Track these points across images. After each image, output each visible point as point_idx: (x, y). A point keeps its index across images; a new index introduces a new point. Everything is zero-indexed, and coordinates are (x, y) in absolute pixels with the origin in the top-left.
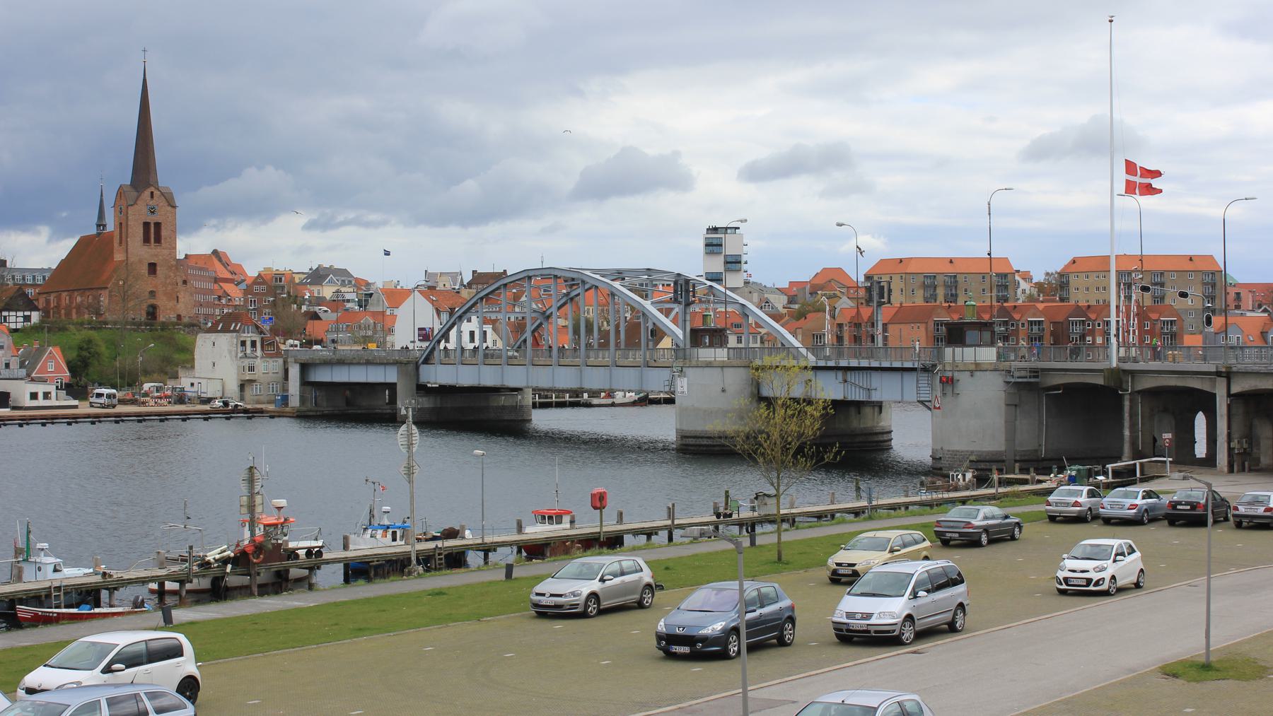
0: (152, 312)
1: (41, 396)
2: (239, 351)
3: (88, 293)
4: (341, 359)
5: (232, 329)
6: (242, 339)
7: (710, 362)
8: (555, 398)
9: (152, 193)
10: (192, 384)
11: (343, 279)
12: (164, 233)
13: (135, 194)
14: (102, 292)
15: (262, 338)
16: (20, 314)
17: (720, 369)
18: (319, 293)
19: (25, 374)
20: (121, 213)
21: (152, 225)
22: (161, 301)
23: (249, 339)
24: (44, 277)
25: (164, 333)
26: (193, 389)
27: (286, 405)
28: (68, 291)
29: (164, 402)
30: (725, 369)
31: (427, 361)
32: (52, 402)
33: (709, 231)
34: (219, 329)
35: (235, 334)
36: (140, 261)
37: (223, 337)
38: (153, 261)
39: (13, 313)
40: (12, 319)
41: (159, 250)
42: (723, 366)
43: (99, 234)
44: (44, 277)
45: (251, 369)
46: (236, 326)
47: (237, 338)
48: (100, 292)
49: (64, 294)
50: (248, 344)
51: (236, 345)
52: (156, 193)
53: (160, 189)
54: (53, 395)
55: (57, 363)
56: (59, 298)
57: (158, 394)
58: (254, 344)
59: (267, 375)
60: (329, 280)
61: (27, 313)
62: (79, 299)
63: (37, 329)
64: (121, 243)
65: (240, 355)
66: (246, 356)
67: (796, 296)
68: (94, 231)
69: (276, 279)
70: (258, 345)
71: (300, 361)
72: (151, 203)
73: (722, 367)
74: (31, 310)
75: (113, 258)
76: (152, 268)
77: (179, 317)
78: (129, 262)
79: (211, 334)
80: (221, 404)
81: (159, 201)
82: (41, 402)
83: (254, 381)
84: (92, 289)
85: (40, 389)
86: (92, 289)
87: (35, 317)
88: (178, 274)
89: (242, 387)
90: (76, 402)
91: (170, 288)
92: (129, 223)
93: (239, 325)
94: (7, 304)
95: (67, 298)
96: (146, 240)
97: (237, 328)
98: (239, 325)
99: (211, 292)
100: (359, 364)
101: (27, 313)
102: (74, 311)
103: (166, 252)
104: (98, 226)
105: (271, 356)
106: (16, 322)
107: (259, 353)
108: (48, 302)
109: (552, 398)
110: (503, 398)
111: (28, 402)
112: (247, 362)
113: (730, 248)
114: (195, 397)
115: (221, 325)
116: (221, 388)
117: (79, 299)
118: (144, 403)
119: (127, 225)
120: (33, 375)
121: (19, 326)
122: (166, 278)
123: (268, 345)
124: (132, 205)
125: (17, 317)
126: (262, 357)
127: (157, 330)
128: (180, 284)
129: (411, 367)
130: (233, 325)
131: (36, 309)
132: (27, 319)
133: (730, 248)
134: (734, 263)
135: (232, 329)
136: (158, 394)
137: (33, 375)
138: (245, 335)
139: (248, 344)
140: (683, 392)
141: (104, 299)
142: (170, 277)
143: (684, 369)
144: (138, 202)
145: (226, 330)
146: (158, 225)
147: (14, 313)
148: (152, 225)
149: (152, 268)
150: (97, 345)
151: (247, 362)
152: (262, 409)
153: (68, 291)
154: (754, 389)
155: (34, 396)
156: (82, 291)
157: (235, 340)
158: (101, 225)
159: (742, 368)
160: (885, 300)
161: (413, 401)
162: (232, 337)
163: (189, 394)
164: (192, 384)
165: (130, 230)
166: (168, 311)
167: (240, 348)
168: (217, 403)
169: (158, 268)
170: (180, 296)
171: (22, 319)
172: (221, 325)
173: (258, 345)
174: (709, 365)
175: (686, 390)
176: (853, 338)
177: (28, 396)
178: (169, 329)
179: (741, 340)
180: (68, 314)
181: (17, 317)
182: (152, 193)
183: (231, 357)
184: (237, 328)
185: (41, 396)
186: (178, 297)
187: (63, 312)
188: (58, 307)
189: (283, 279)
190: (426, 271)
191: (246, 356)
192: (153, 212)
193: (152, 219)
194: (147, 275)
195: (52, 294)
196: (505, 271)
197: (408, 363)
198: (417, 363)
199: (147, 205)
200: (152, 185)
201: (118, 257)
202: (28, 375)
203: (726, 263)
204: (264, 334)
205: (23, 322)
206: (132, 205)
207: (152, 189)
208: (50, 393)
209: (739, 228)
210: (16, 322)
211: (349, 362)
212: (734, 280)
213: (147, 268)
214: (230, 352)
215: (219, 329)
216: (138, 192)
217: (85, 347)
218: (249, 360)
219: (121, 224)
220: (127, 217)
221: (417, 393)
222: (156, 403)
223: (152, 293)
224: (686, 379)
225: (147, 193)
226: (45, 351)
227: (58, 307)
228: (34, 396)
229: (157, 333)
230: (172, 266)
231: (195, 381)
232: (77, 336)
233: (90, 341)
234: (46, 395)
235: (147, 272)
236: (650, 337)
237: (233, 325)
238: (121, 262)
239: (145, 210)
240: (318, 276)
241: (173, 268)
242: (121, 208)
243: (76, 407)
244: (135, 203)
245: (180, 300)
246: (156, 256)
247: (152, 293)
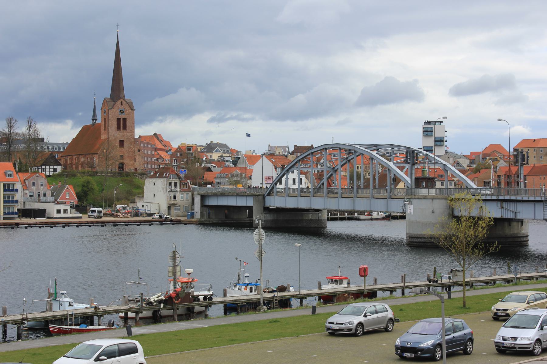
0: (122, 166)
1: (62, 211)
2: (168, 188)
3: (87, 156)
4: (223, 193)
5: (164, 176)
6: (170, 182)
7: (426, 196)
8: (340, 215)
9: (122, 102)
10: (143, 206)
11: (224, 149)
12: (128, 124)
13: (113, 103)
14: (95, 156)
15: (180, 181)
16: (51, 167)
17: (431, 200)
18: (211, 157)
19: (54, 199)
20: (105, 113)
21: (122, 120)
22: (126, 161)
23: (173, 182)
24: (64, 148)
25: (128, 178)
26: (143, 209)
27: (193, 217)
28: (77, 155)
29: (128, 215)
30: (434, 200)
31: (269, 195)
32: (69, 215)
33: (426, 124)
34: (157, 176)
35: (166, 179)
36: (115, 139)
37: (159, 180)
38: (122, 139)
39: (47, 167)
40: (47, 170)
41: (125, 133)
42: (433, 199)
43: (93, 125)
44: (64, 148)
45: (174, 198)
46: (166, 175)
47: (167, 181)
48: (94, 156)
49: (75, 157)
50: (173, 184)
51: (166, 185)
52: (124, 102)
53: (126, 100)
54: (69, 211)
55: (71, 194)
56: (72, 159)
57: (125, 211)
58: (176, 184)
59: (182, 201)
60: (216, 150)
61: (55, 167)
62: (83, 159)
63: (60, 175)
64: (105, 129)
65: (168, 190)
66: (171, 191)
67: (474, 160)
68: (90, 123)
69: (188, 149)
70: (178, 185)
71: (201, 194)
72: (121, 108)
73: (433, 199)
74: (57, 165)
75: (101, 137)
76: (122, 143)
77: (136, 169)
78: (109, 140)
79: (153, 179)
80: (158, 217)
81: (125, 107)
82: (62, 215)
83: (176, 204)
84: (90, 154)
85: (62, 207)
86: (90, 154)
87: (59, 169)
88: (135, 146)
89: (169, 207)
90: (81, 215)
91: (131, 154)
92: (109, 119)
93: (168, 174)
94: (45, 162)
95: (77, 159)
96: (118, 128)
97: (167, 176)
98: (168, 174)
99: (153, 156)
100: (232, 195)
101: (55, 167)
102: (80, 166)
103: (129, 134)
104: (93, 120)
105: (185, 191)
106: (49, 172)
107: (178, 189)
108: (66, 161)
109: (338, 215)
110: (311, 215)
111: (56, 215)
112: (172, 194)
113: (438, 133)
114: (144, 213)
115: (158, 174)
116: (158, 208)
117: (83, 159)
118: (117, 216)
119: (108, 120)
120: (58, 200)
121: (51, 174)
122: (129, 148)
123: (183, 185)
124: (111, 109)
125: (50, 169)
126: (180, 191)
127: (124, 176)
128: (136, 151)
129: (261, 198)
130: (165, 174)
131: (60, 165)
132: (55, 170)
133: (438, 133)
134: (439, 141)
135: (164, 176)
136: (125, 211)
137: (58, 200)
138: (171, 179)
139: (173, 184)
140: (410, 213)
141: (96, 160)
142: (131, 147)
143: (411, 200)
144: (114, 107)
145: (161, 177)
146: (125, 120)
147: (48, 167)
148: (122, 120)
149: (122, 143)
150: (92, 184)
151: (172, 194)
152: (180, 219)
153: (77, 155)
154: (450, 212)
155: (59, 211)
156: (84, 155)
157: (166, 182)
158: (94, 119)
159: (443, 200)
160: (525, 162)
161: (262, 216)
162: (164, 181)
163: (141, 211)
164: (143, 206)
165: (110, 123)
166: (130, 166)
167: (168, 187)
168: (156, 216)
169: (125, 143)
170: (136, 158)
171: (52, 170)
172: (158, 174)
173: (178, 185)
174: (425, 198)
175: (412, 211)
176: (506, 183)
177: (56, 211)
178: (131, 176)
179: (443, 184)
180: (77, 168)
181: (50, 169)
182: (122, 102)
183: (164, 191)
184: (167, 176)
185: (62, 211)
186: (135, 158)
187: (74, 166)
188: (71, 164)
189: (192, 149)
190: (269, 145)
191: (172, 191)
192: (122, 113)
193: (122, 116)
194: (119, 147)
195: (68, 157)
196: (312, 145)
197: (259, 195)
198: (264, 195)
199: (119, 109)
200: (122, 98)
201: (104, 137)
202: (56, 200)
203: (435, 141)
204: (181, 179)
205: (53, 172)
206: (111, 109)
207: (122, 100)
208: (67, 210)
209: (442, 122)
210: (49, 172)
211: (227, 194)
212: (440, 151)
213: (119, 143)
214: (163, 188)
215: (157, 176)
216: (114, 102)
217: (86, 185)
218: (173, 193)
219: (105, 119)
220: (108, 116)
221: (264, 212)
222: (123, 216)
223: (122, 157)
224: (412, 205)
225: (119, 102)
226: (64, 187)
227: (71, 164)
228: (59, 211)
229: (124, 178)
230: (132, 142)
231: (144, 204)
232: (82, 179)
233: (88, 182)
234: (65, 211)
235: (119, 145)
236: (392, 182)
237: (165, 174)
238: (105, 139)
239: (118, 111)
240: (210, 147)
241: (133, 143)
242: (105, 111)
243: (81, 217)
244: (113, 108)
245: (136, 160)
246: (124, 136)
247: (122, 157)
